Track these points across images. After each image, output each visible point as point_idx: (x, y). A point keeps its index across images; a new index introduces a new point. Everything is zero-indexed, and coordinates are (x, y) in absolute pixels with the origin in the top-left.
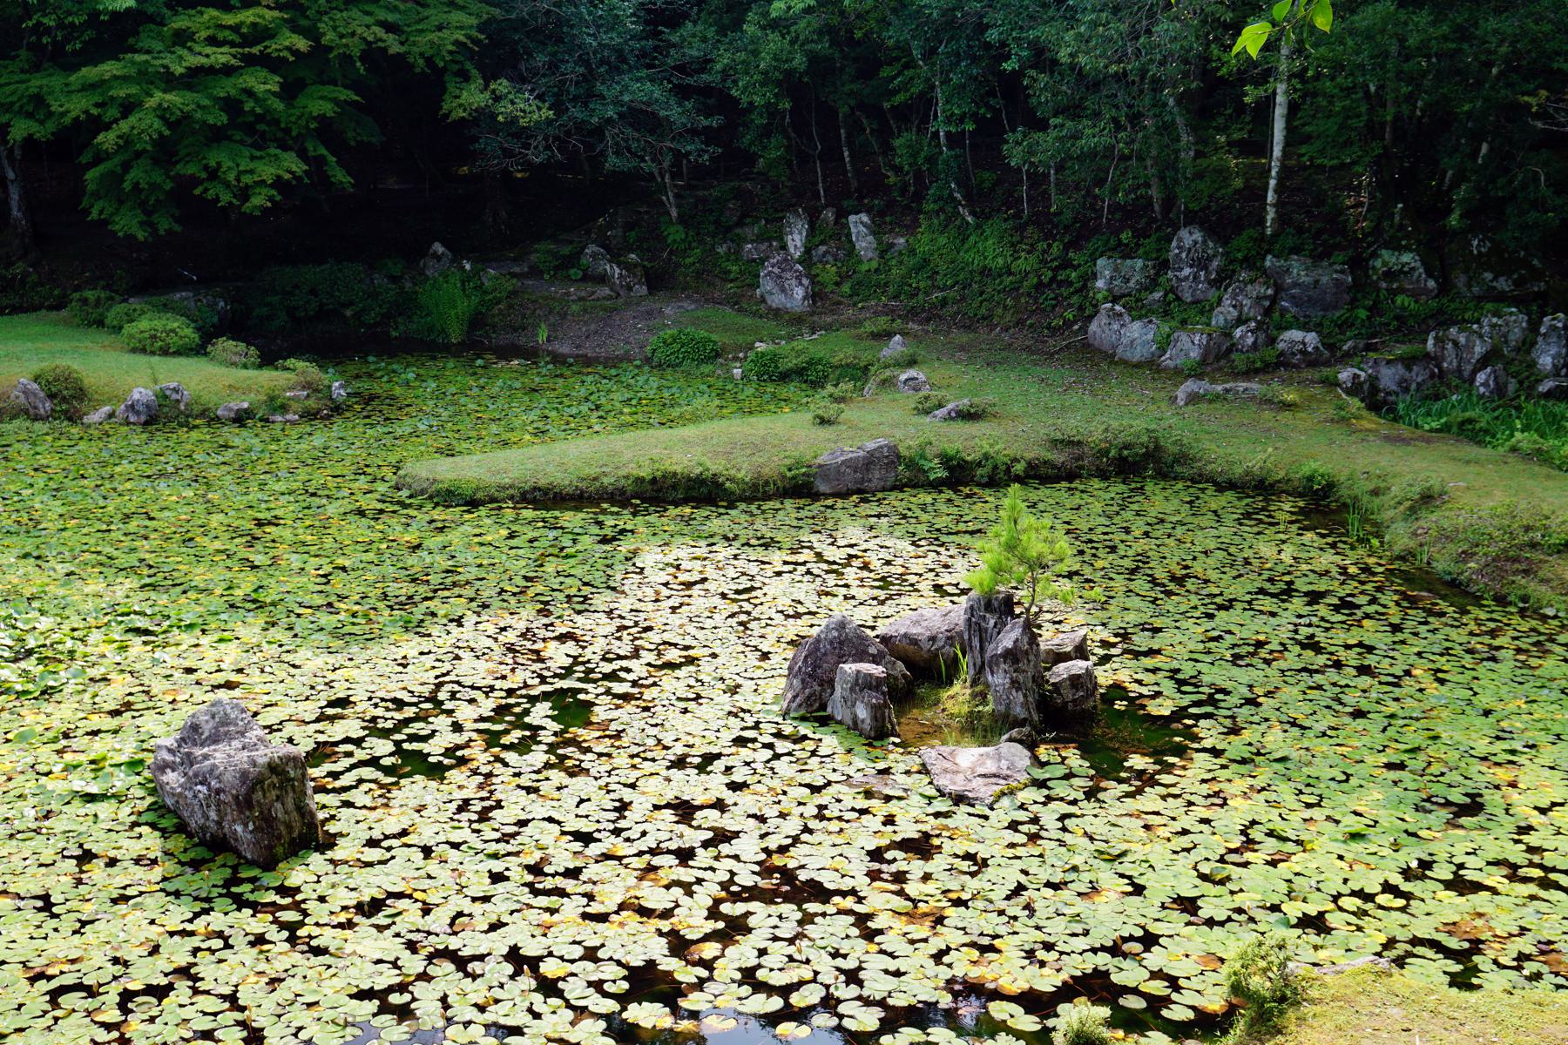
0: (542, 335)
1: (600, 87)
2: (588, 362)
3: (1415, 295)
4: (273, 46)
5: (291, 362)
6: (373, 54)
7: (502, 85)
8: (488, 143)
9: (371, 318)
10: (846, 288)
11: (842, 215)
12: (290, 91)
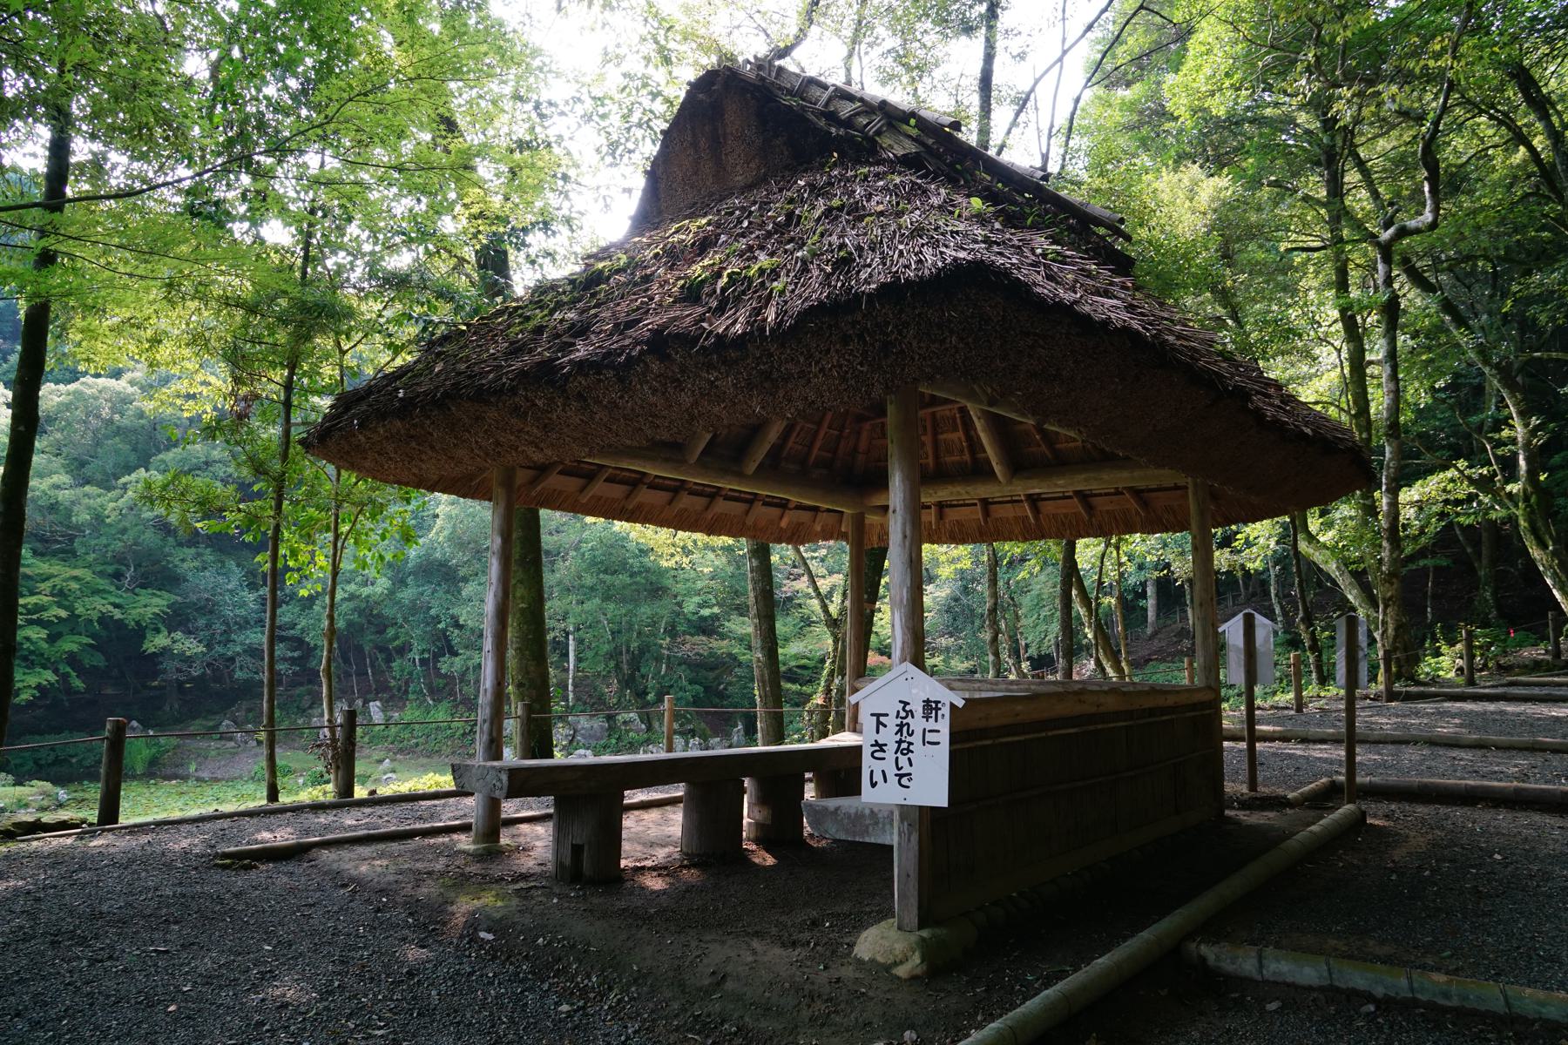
0: (192, 768)
1: (233, 636)
2: (216, 780)
3: (637, 732)
4: (45, 615)
5: (34, 782)
6: (104, 620)
7: (178, 635)
8: (169, 665)
9: (87, 763)
10: (366, 739)
11: (366, 702)
12: (52, 639)
